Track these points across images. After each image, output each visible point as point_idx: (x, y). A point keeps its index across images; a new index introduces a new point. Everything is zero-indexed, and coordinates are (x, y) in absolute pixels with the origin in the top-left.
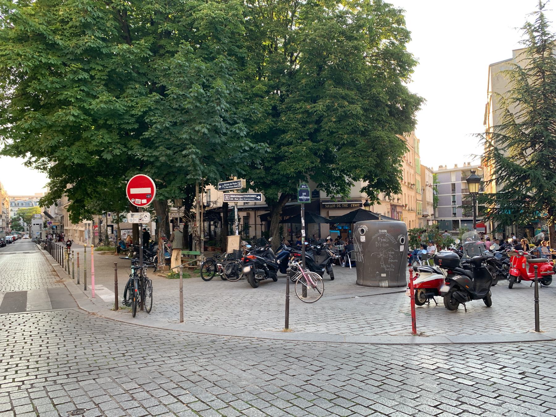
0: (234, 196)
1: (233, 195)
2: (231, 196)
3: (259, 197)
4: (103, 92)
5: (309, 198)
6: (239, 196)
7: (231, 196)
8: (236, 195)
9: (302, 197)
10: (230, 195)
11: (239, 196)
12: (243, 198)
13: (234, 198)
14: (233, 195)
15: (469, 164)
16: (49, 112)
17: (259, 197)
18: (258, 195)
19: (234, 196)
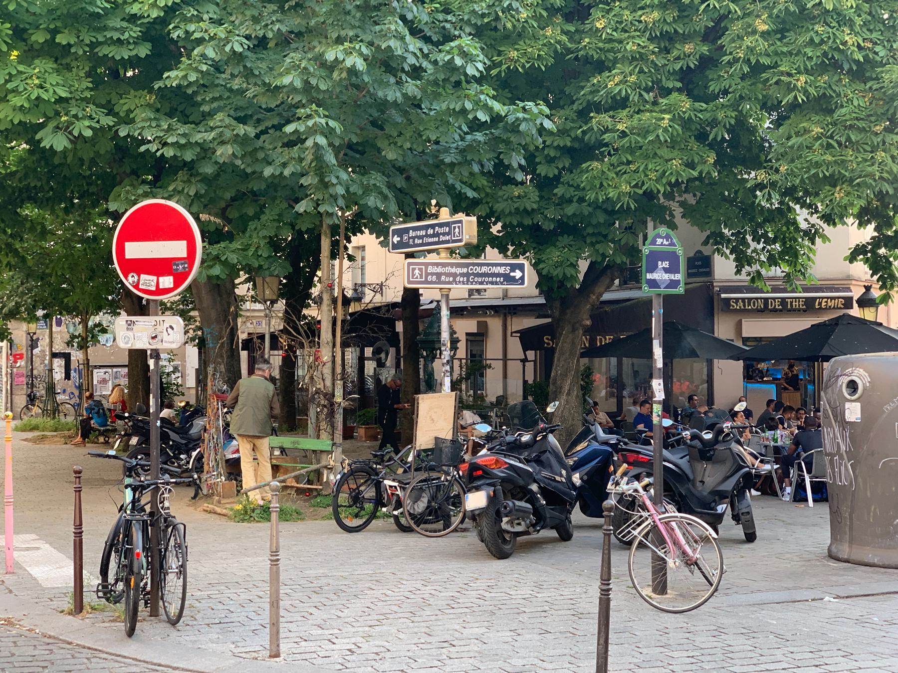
3: (518, 274)
6: (453, 270)
7: (430, 269)
10: (427, 265)
11: (453, 270)
12: (467, 275)
13: (439, 275)
17: (518, 274)
18: (513, 267)
19: (439, 270)
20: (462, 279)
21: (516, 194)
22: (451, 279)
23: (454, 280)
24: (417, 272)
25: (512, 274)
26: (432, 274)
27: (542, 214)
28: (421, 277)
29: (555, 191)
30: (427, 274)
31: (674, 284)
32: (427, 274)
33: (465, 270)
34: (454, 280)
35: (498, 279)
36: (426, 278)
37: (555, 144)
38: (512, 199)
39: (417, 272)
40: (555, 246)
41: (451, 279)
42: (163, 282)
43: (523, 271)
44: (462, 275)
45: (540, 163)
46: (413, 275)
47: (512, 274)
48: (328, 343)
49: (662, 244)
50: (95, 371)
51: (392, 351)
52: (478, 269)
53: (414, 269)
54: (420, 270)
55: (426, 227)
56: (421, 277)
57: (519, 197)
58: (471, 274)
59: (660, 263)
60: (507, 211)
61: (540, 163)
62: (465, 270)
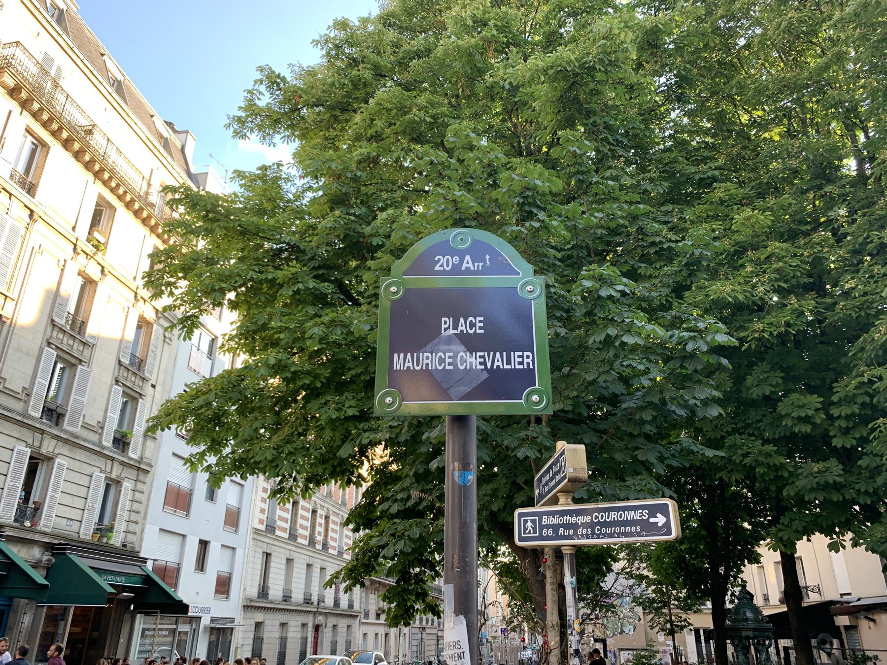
0: (556, 520)
1: (553, 514)
2: (545, 520)
3: (660, 520)
4: (302, 238)
5: (520, 360)
6: (573, 520)
7: (545, 520)
8: (562, 513)
9: (429, 360)
10: (540, 515)
11: (573, 520)
12: (592, 525)
13: (556, 528)
14: (553, 514)
15: (834, 547)
16: (366, 543)
17: (660, 520)
18: (653, 511)
19: (556, 520)
20: (585, 531)
21: (816, 469)
22: (571, 532)
23: (556, 531)
24: (529, 524)
25: (652, 520)
26: (548, 527)
27: (853, 488)
28: (535, 532)
29: (859, 463)
30: (542, 527)
31: (498, 383)
32: (542, 527)
33: (588, 519)
34: (556, 531)
35: (633, 529)
36: (541, 532)
37: (843, 414)
38: (811, 474)
39: (529, 524)
40: (881, 523)
41: (571, 532)
42: (86, 535)
43: (666, 514)
44: (585, 525)
45: (835, 436)
46: (525, 529)
47: (652, 520)
48: (553, 627)
49: (456, 270)
50: (622, 652)
51: (835, 641)
52: (605, 516)
53: (526, 522)
54: (533, 522)
55: (547, 471)
56: (535, 532)
57: (819, 472)
58: (599, 523)
59: (446, 322)
60: (809, 487)
61: (835, 436)
62: (588, 519)
